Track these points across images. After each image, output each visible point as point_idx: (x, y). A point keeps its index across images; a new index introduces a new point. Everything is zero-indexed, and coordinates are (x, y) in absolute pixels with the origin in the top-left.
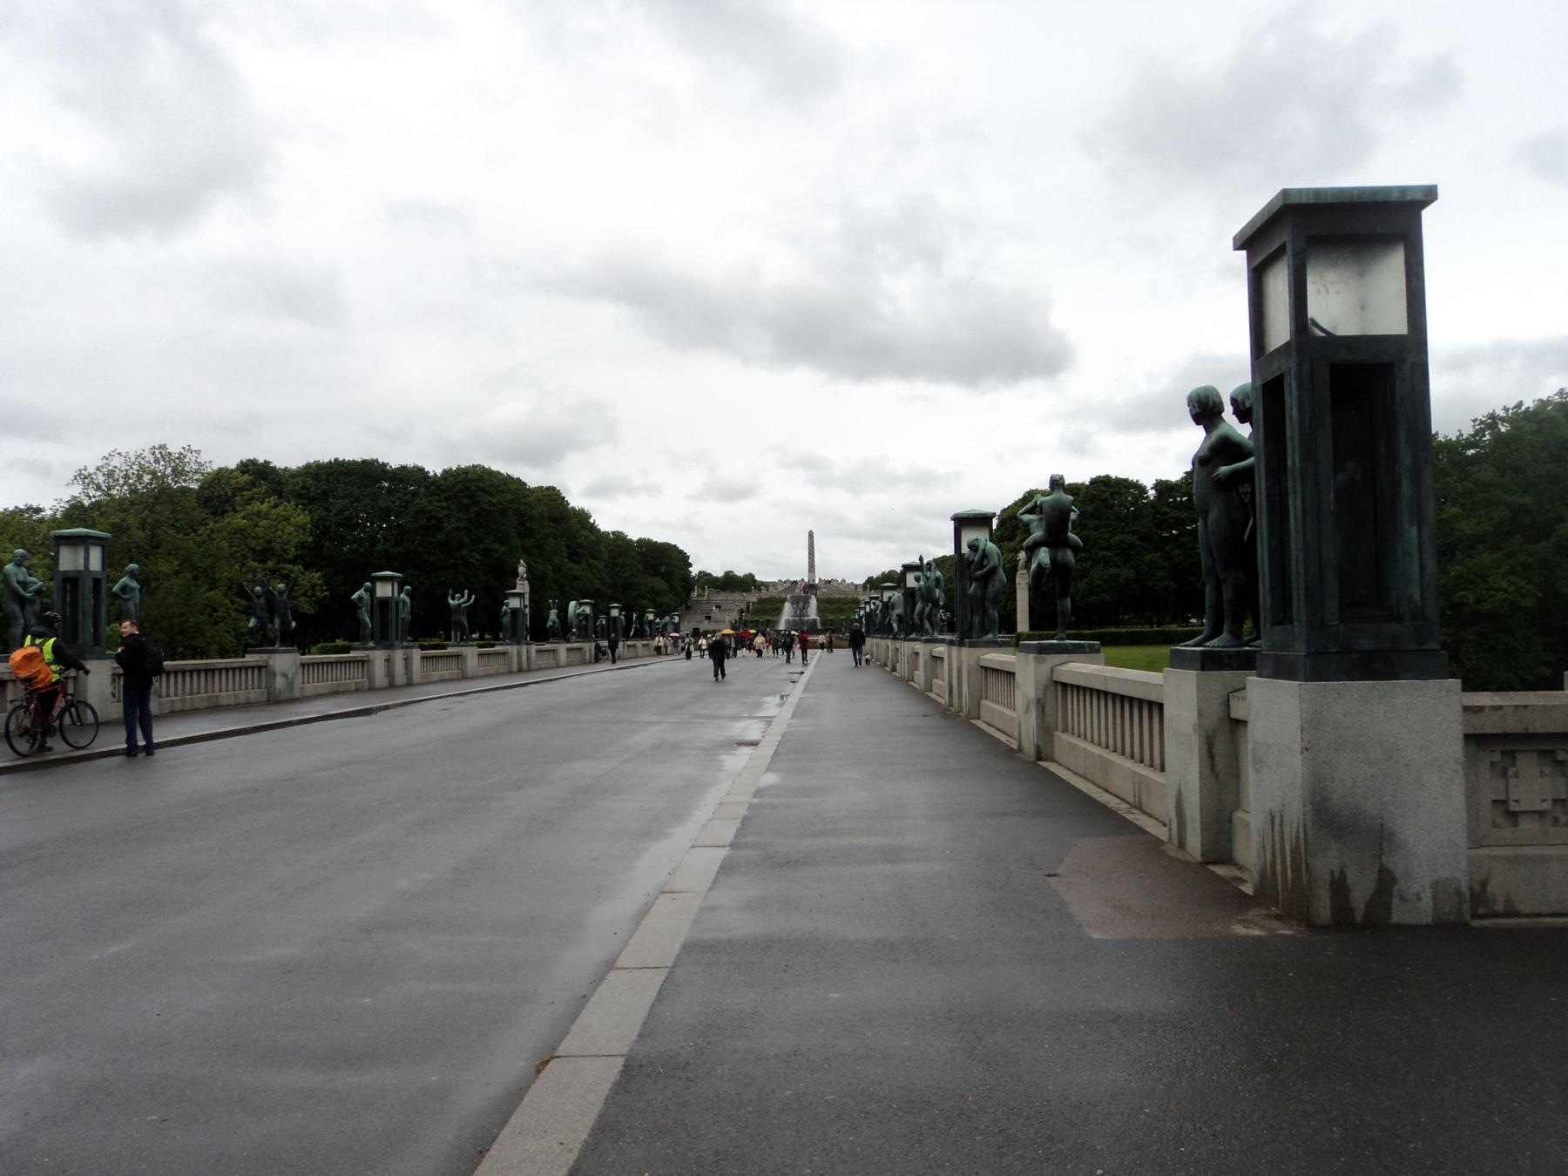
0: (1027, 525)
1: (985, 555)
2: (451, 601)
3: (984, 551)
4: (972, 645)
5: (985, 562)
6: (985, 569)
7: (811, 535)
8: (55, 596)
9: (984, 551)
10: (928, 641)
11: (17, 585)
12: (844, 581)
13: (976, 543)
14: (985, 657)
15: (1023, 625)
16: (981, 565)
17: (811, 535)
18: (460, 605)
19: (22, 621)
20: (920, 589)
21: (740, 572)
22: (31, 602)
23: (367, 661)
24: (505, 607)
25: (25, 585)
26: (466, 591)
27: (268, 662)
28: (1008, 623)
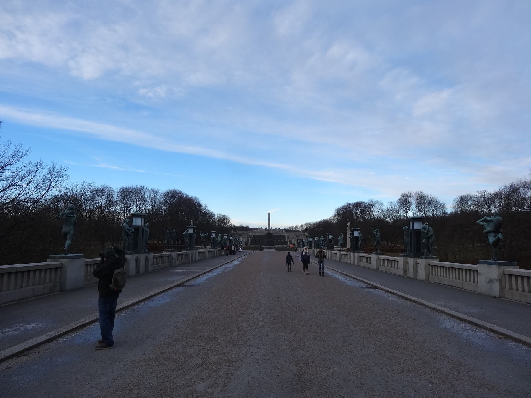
0: (482, 226)
1: (428, 231)
2: (201, 235)
3: (428, 229)
4: (330, 250)
5: (429, 233)
6: (429, 235)
7: (269, 214)
8: (144, 234)
9: (428, 229)
10: (377, 254)
11: (127, 230)
12: (279, 228)
13: (425, 227)
14: (507, 269)
15: (348, 246)
16: (427, 234)
17: (269, 214)
18: (204, 236)
19: (128, 242)
20: (361, 237)
21: (245, 225)
22: (131, 235)
23: (188, 254)
24: (211, 237)
25: (129, 230)
26: (206, 232)
27: (171, 254)
28: (344, 245)
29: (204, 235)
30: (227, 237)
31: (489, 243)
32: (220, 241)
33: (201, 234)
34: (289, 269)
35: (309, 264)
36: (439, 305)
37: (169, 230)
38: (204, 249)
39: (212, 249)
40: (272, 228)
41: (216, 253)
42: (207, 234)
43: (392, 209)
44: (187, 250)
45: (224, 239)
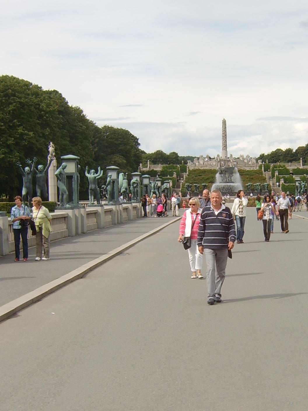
2: (87, 175)
7: (224, 122)
17: (224, 122)
18: (95, 177)
23: (128, 208)
29: (96, 175)
30: (139, 180)
31: (156, 199)
32: (126, 189)
33: (89, 173)
34: (267, 239)
35: (68, 104)
36: (297, 216)
37: (30, 166)
38: (95, 206)
39: (112, 205)
40: (231, 155)
41: (52, 222)
42: (100, 174)
43: (274, 186)
44: (66, 209)
45: (134, 183)
